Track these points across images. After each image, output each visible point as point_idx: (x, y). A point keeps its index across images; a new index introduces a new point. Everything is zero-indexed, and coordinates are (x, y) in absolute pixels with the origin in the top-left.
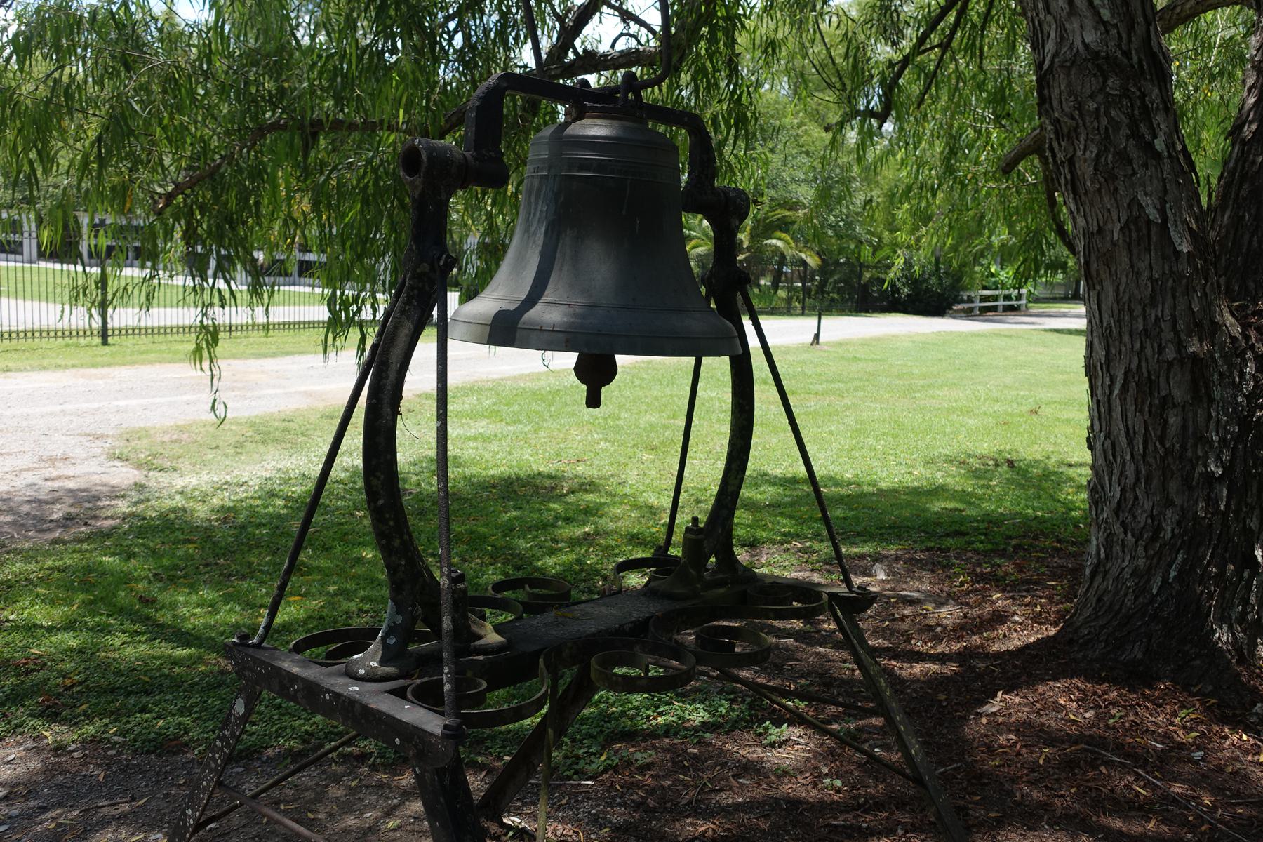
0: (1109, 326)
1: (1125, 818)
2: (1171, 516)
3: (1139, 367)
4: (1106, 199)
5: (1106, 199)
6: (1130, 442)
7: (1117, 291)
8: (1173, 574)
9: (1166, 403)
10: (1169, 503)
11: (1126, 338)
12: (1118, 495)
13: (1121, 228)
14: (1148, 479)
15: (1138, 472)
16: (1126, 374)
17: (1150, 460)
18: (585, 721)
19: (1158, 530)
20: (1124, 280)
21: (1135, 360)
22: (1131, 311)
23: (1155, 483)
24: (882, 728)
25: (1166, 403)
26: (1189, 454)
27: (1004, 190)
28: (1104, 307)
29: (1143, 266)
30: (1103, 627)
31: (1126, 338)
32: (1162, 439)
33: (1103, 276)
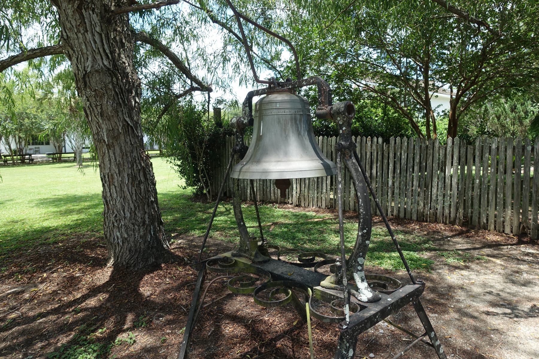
0: (119, 161)
1: (101, 326)
2: (147, 216)
3: (131, 173)
4: (115, 118)
5: (115, 118)
6: (131, 196)
7: (121, 149)
8: (152, 233)
9: (140, 182)
10: (146, 212)
11: (126, 164)
12: (129, 215)
13: (122, 128)
14: (138, 206)
15: (135, 206)
16: (128, 175)
17: (138, 201)
18: (374, 311)
19: (145, 221)
20: (123, 145)
21: (130, 171)
22: (127, 155)
23: (140, 208)
24: (138, 316)
25: (140, 182)
26: (147, 196)
27: (508, 67)
28: (116, 155)
29: (128, 140)
30: (137, 258)
31: (126, 164)
32: (140, 194)
33: (115, 144)
